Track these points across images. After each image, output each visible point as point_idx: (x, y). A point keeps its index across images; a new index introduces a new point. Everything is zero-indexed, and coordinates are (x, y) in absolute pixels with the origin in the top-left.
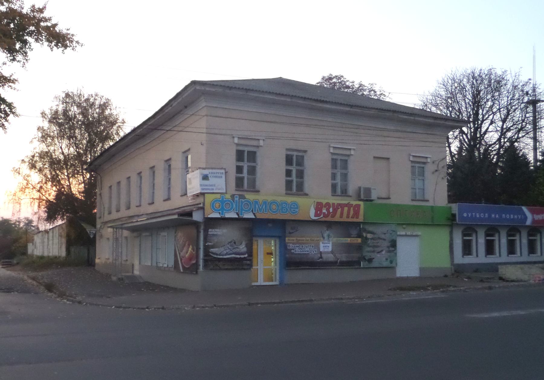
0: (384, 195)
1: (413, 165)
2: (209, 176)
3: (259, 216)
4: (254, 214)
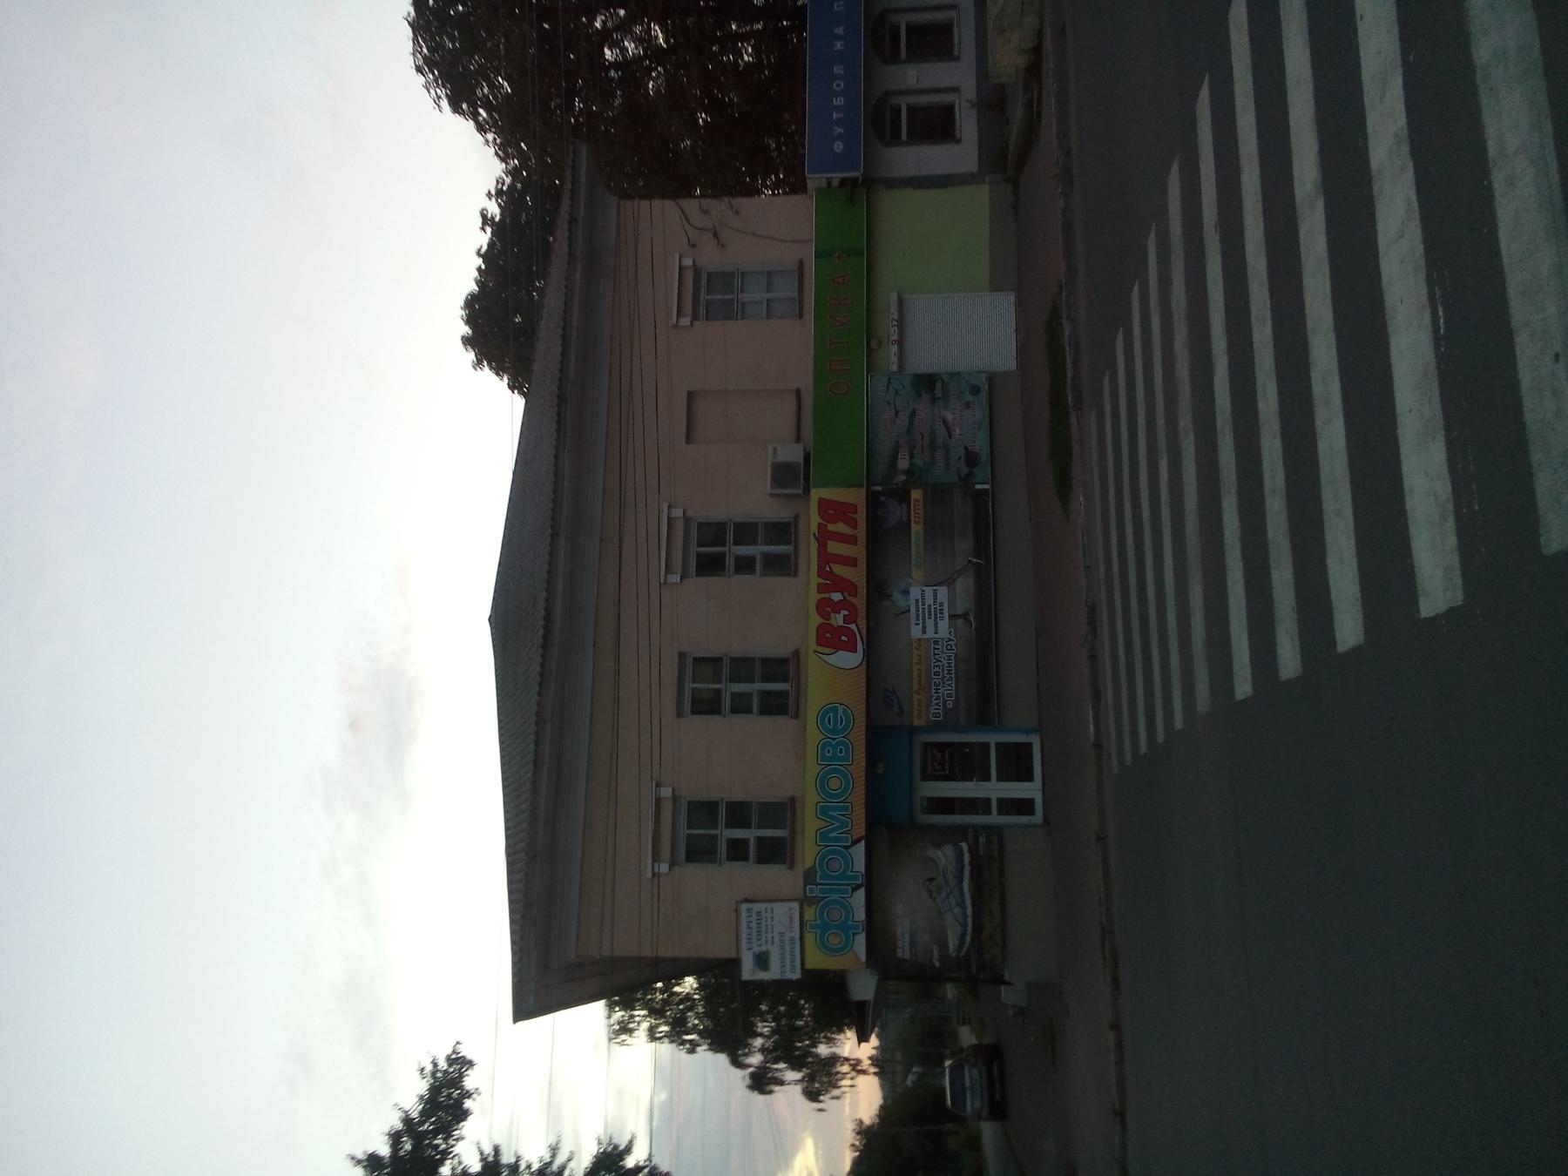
0: (789, 406)
1: (702, 311)
2: (757, 950)
3: (860, 830)
4: (855, 842)
